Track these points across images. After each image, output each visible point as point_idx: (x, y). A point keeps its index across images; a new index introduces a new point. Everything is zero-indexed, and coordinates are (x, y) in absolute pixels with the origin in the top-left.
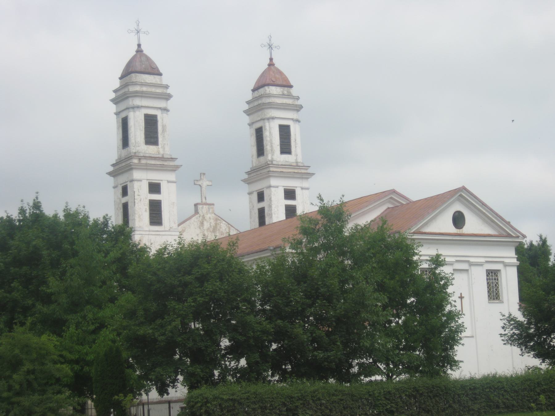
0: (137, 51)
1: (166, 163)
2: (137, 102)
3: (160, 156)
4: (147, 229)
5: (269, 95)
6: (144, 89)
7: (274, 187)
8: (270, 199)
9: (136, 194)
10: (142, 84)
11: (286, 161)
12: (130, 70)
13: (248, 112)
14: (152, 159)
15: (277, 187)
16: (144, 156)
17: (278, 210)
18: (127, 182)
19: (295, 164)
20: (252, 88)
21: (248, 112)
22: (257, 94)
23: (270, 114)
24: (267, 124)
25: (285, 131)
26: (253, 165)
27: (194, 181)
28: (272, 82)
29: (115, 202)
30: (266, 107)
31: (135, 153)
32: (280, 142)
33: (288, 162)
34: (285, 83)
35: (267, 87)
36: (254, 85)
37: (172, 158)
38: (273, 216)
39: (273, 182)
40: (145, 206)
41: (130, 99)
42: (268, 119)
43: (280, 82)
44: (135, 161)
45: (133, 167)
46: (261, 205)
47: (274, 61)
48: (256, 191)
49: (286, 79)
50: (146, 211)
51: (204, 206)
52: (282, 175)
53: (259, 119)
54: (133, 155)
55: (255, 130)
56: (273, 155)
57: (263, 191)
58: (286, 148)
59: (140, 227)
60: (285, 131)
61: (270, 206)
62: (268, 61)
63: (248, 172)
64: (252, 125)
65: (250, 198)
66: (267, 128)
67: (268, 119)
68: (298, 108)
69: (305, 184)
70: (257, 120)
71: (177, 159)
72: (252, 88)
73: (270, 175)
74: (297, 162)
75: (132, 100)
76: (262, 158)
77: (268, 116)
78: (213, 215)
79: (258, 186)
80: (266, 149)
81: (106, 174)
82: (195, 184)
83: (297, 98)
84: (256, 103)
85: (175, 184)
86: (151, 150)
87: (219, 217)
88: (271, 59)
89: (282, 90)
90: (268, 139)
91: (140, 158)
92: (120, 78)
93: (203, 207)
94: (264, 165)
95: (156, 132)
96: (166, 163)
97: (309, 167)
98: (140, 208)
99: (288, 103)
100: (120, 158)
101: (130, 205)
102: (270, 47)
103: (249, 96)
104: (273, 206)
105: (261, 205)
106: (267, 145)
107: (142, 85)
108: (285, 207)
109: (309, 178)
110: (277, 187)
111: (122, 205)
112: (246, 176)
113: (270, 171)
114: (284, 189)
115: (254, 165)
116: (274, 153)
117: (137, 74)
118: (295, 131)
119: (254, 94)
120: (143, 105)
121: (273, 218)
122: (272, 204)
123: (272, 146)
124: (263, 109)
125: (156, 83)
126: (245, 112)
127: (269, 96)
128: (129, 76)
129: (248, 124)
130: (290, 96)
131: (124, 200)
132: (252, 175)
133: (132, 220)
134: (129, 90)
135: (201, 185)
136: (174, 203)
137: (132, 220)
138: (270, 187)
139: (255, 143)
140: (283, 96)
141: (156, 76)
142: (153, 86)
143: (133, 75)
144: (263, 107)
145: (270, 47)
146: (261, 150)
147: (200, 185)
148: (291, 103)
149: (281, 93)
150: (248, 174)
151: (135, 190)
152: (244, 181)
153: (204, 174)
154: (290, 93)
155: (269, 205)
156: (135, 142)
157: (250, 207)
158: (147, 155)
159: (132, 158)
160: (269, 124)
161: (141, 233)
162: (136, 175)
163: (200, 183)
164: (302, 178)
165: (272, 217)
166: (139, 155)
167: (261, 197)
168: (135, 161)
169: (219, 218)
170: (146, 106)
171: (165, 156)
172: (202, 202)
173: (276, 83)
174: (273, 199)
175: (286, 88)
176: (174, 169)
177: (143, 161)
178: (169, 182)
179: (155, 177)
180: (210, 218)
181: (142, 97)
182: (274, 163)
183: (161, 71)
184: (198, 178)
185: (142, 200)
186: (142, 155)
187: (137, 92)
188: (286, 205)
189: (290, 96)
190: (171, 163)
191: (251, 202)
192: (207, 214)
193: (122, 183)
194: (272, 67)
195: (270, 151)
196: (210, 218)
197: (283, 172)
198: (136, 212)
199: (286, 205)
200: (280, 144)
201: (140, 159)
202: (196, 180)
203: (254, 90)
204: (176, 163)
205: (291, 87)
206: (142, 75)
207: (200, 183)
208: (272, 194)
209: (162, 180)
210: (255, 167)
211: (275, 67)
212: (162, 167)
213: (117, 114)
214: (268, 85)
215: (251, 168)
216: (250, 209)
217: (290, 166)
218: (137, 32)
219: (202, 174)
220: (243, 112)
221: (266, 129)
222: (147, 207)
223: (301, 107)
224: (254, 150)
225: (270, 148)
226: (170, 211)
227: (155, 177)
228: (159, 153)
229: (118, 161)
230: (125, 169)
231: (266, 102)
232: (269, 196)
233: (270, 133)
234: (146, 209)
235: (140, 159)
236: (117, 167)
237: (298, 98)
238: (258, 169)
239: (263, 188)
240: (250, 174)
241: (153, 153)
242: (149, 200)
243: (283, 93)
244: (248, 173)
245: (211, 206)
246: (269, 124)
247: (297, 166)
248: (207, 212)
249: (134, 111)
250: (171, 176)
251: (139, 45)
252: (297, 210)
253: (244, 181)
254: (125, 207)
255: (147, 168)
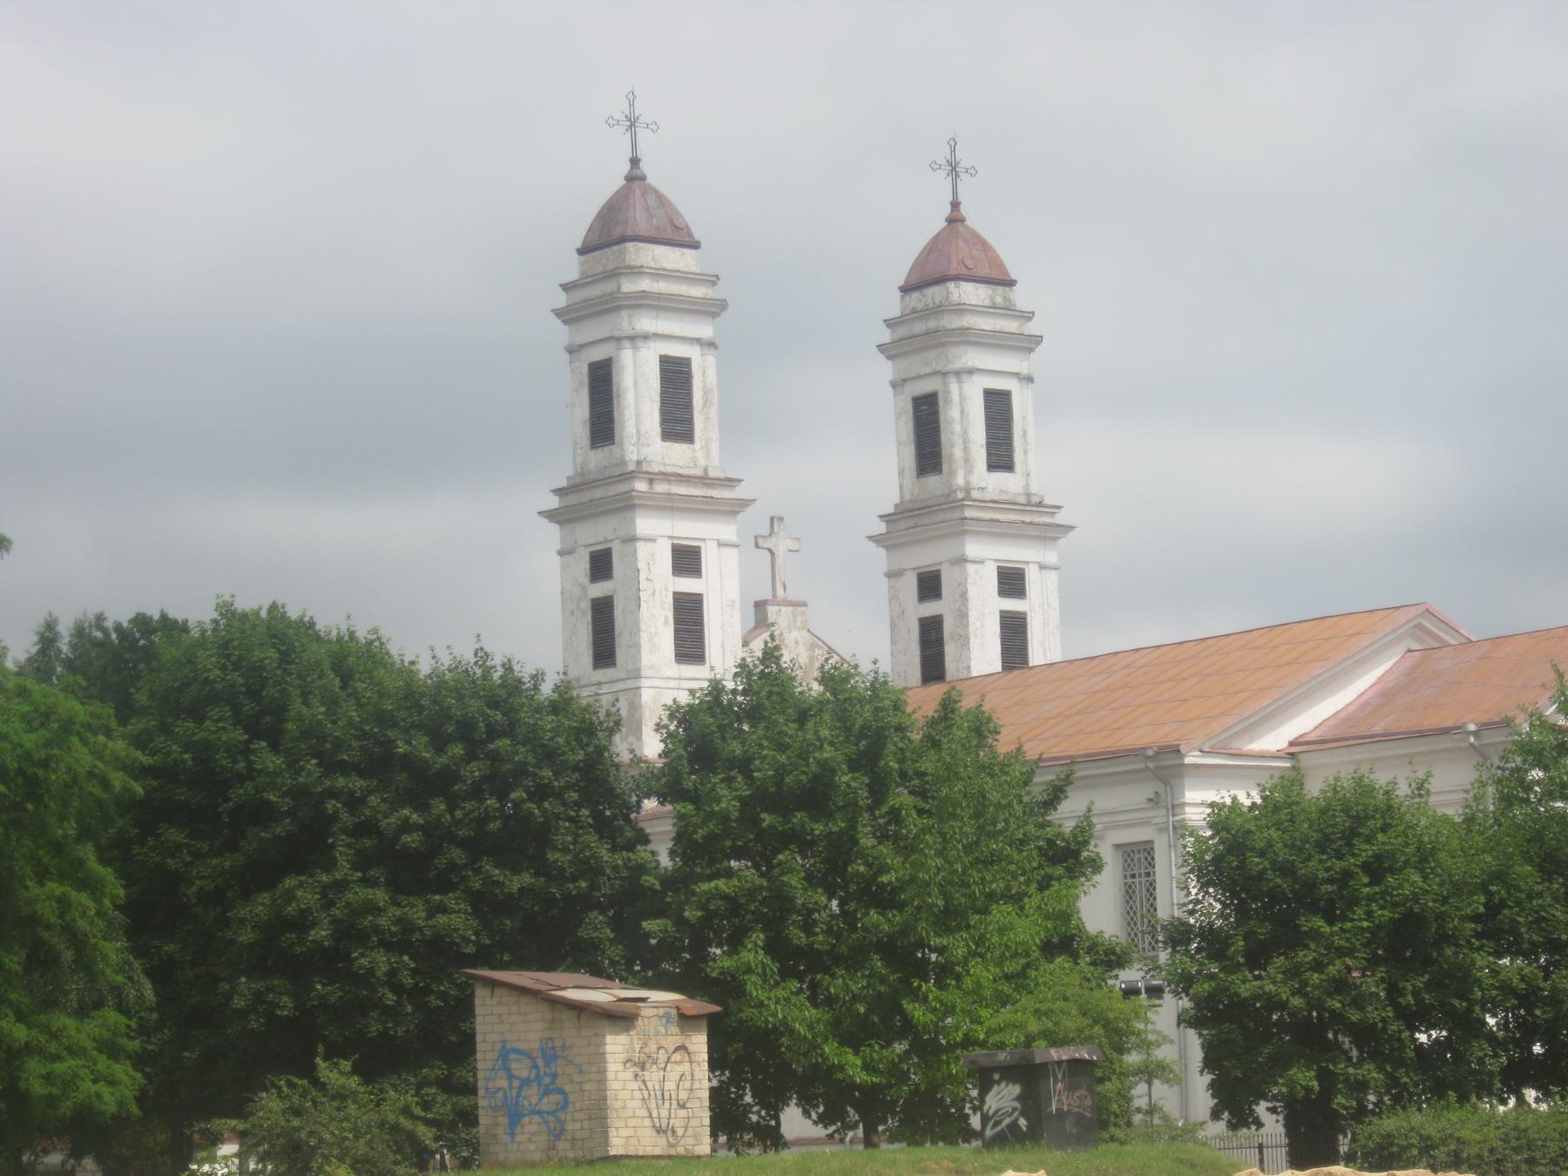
0: (630, 179)
1: (715, 493)
2: (646, 322)
3: (699, 472)
4: (670, 674)
5: (961, 307)
6: (662, 286)
7: (973, 562)
8: (964, 595)
9: (643, 576)
10: (660, 274)
11: (1001, 491)
12: (617, 232)
13: (568, 316)
14: (681, 481)
15: (981, 562)
16: (662, 473)
17: (983, 626)
18: (612, 540)
19: (1022, 500)
20: (901, 282)
21: (568, 316)
22: (915, 299)
23: (964, 359)
24: (954, 387)
25: (675, 376)
26: (902, 497)
27: (756, 537)
28: (965, 271)
29: (562, 593)
30: (954, 339)
31: (639, 463)
32: (988, 437)
33: (1006, 492)
34: (996, 275)
35: (953, 283)
36: (906, 272)
37: (729, 480)
38: (971, 642)
39: (973, 548)
40: (663, 608)
41: (624, 314)
42: (958, 374)
43: (984, 272)
44: (641, 486)
45: (636, 502)
46: (930, 609)
47: (963, 210)
48: (914, 569)
49: (997, 263)
50: (666, 623)
51: (783, 609)
52: (995, 530)
53: (928, 370)
54: (631, 467)
55: (910, 399)
56: (969, 472)
57: (939, 571)
58: (677, 424)
59: (652, 667)
60: (998, 406)
61: (963, 615)
62: (947, 210)
63: (889, 515)
64: (903, 385)
65: (892, 587)
66: (955, 397)
67: (958, 374)
68: (1029, 344)
69: (1050, 556)
70: (922, 373)
71: (742, 481)
72: (580, 246)
73: (966, 528)
74: (1028, 495)
75: (630, 316)
76: (933, 481)
77: (958, 365)
78: (805, 633)
79: (924, 557)
80: (951, 455)
81: (538, 516)
82: (757, 546)
83: (714, 279)
84: (918, 327)
85: (734, 551)
86: (675, 456)
87: (819, 639)
88: (955, 205)
89: (990, 292)
90: (957, 428)
91: (653, 476)
92: (583, 251)
93: (780, 610)
94: (943, 500)
95: (689, 406)
96: (715, 493)
97: (1059, 507)
98: (653, 616)
99: (1007, 330)
100: (583, 474)
101: (948, 627)
102: (954, 169)
103: (572, 268)
104: (972, 615)
105: (930, 609)
106: (952, 446)
107: (657, 275)
108: (1001, 617)
109: (1058, 538)
110: (981, 562)
111: (590, 604)
112: (881, 528)
113: (965, 518)
114: (673, 545)
115: (908, 497)
116: (972, 467)
117: (641, 244)
118: (705, 373)
119: (907, 298)
120: (660, 331)
121: (971, 645)
122: (970, 607)
123: (966, 449)
124: (944, 344)
125: (686, 269)
126: (558, 313)
127: (961, 309)
128: (616, 248)
129: (891, 382)
130: (1008, 310)
131: (599, 590)
132: (902, 525)
133: (630, 647)
134: (619, 288)
135: (774, 550)
136: (733, 601)
137: (630, 647)
138: (962, 560)
139: (912, 436)
140: (994, 309)
141: (685, 251)
142: (681, 277)
143: (630, 246)
144: (944, 340)
145: (954, 169)
146: (603, 427)
147: (770, 550)
148: (1014, 331)
149: (987, 302)
150: (887, 522)
151: (640, 566)
152: (550, 515)
153: (781, 519)
154: (1010, 301)
155: (960, 610)
156: (638, 432)
157: (891, 611)
158: (669, 470)
159: (633, 478)
160: (960, 388)
161: (656, 683)
162: (645, 524)
163: (769, 544)
164: (1045, 539)
165: (969, 643)
166: (650, 470)
167: (929, 586)
168: (641, 486)
169: (820, 643)
170: (666, 333)
171: (713, 473)
172: (774, 595)
173: (973, 273)
174: (970, 595)
175: (1000, 289)
176: (734, 509)
177: (660, 488)
178: (721, 544)
179: (1014, 553)
180: (797, 642)
181: (658, 308)
182: (975, 494)
183: (697, 236)
184: (766, 531)
185: (657, 593)
186: (655, 469)
187: (644, 294)
188: (1002, 612)
189: (1008, 310)
190: (727, 494)
191: (894, 597)
192: (790, 632)
193: (591, 541)
194: (637, 184)
195: (962, 461)
196: (797, 642)
197: (998, 521)
198: (643, 627)
199: (1002, 612)
200: (988, 443)
201: (651, 481)
202: (761, 536)
203: (906, 290)
204: (739, 493)
205: (1010, 283)
206: (650, 246)
207: (769, 544)
208: (969, 580)
209: (705, 540)
210: (911, 501)
211: (967, 228)
212: (708, 504)
213: (573, 350)
214: (957, 278)
215: (896, 505)
216: (892, 619)
217: (1010, 504)
218: (629, 123)
219: (775, 520)
220: (876, 349)
221: (948, 401)
222: (669, 613)
223: (1037, 340)
224: (582, 432)
225: (962, 454)
226: (723, 625)
227: (689, 529)
228: (695, 466)
229: (578, 480)
230: (607, 508)
231: (953, 326)
232: (960, 584)
233: (962, 412)
234: (666, 617)
235: (651, 481)
236: (573, 499)
237: (1028, 316)
238: (923, 508)
239: (941, 563)
240: (894, 521)
241: (682, 464)
242: (675, 593)
243: (992, 301)
244: (888, 518)
245: (799, 609)
246: (960, 388)
247: (1029, 504)
248: (789, 626)
249: (635, 348)
250: (727, 530)
251: (635, 162)
252: (1029, 627)
253: (550, 515)
254: (603, 612)
255: (998, 531)
